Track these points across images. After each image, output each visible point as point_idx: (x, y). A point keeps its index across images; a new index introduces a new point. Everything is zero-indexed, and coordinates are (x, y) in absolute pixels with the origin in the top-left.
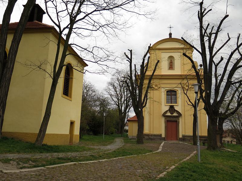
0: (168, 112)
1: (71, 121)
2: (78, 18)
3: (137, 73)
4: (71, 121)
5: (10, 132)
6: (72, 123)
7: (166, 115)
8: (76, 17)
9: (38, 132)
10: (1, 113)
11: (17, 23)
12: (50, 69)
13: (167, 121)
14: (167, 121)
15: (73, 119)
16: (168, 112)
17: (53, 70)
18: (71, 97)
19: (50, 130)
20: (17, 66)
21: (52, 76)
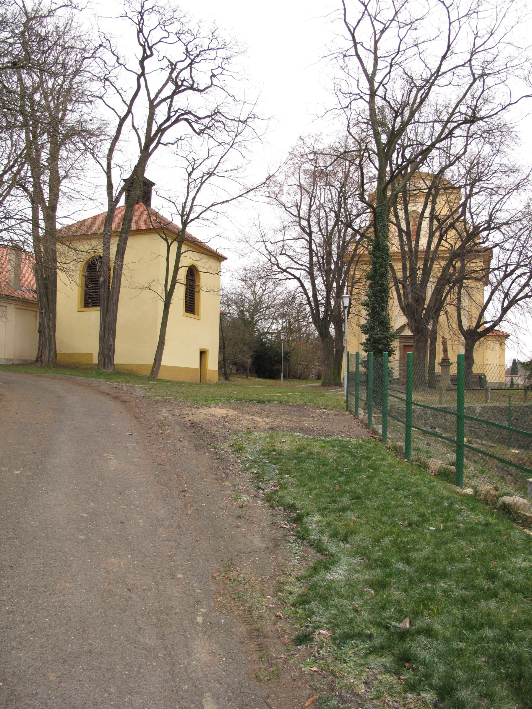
0: (407, 328)
1: (201, 349)
2: (192, 216)
3: (470, 204)
4: (201, 349)
5: (122, 364)
6: (203, 353)
7: (403, 334)
8: (188, 215)
9: (152, 363)
10: (112, 341)
11: (143, 173)
12: (161, 290)
13: (404, 346)
14: (404, 346)
15: (204, 347)
16: (407, 328)
17: (164, 289)
18: (198, 315)
19: (165, 361)
20: (123, 291)
21: (164, 297)
